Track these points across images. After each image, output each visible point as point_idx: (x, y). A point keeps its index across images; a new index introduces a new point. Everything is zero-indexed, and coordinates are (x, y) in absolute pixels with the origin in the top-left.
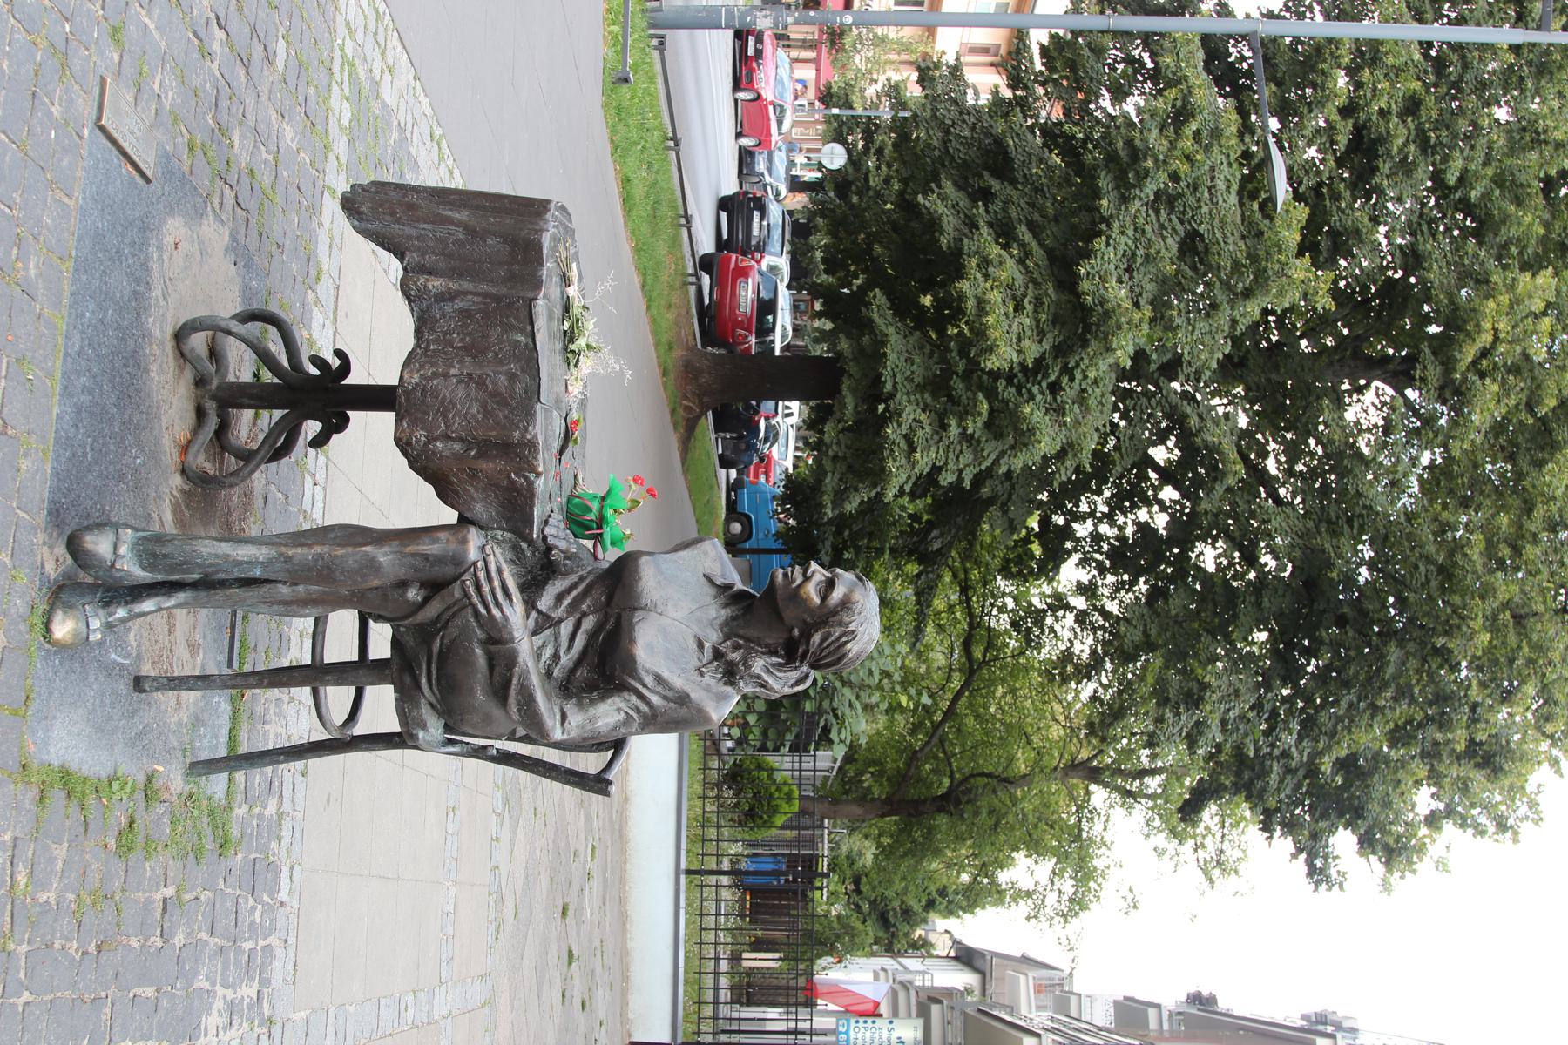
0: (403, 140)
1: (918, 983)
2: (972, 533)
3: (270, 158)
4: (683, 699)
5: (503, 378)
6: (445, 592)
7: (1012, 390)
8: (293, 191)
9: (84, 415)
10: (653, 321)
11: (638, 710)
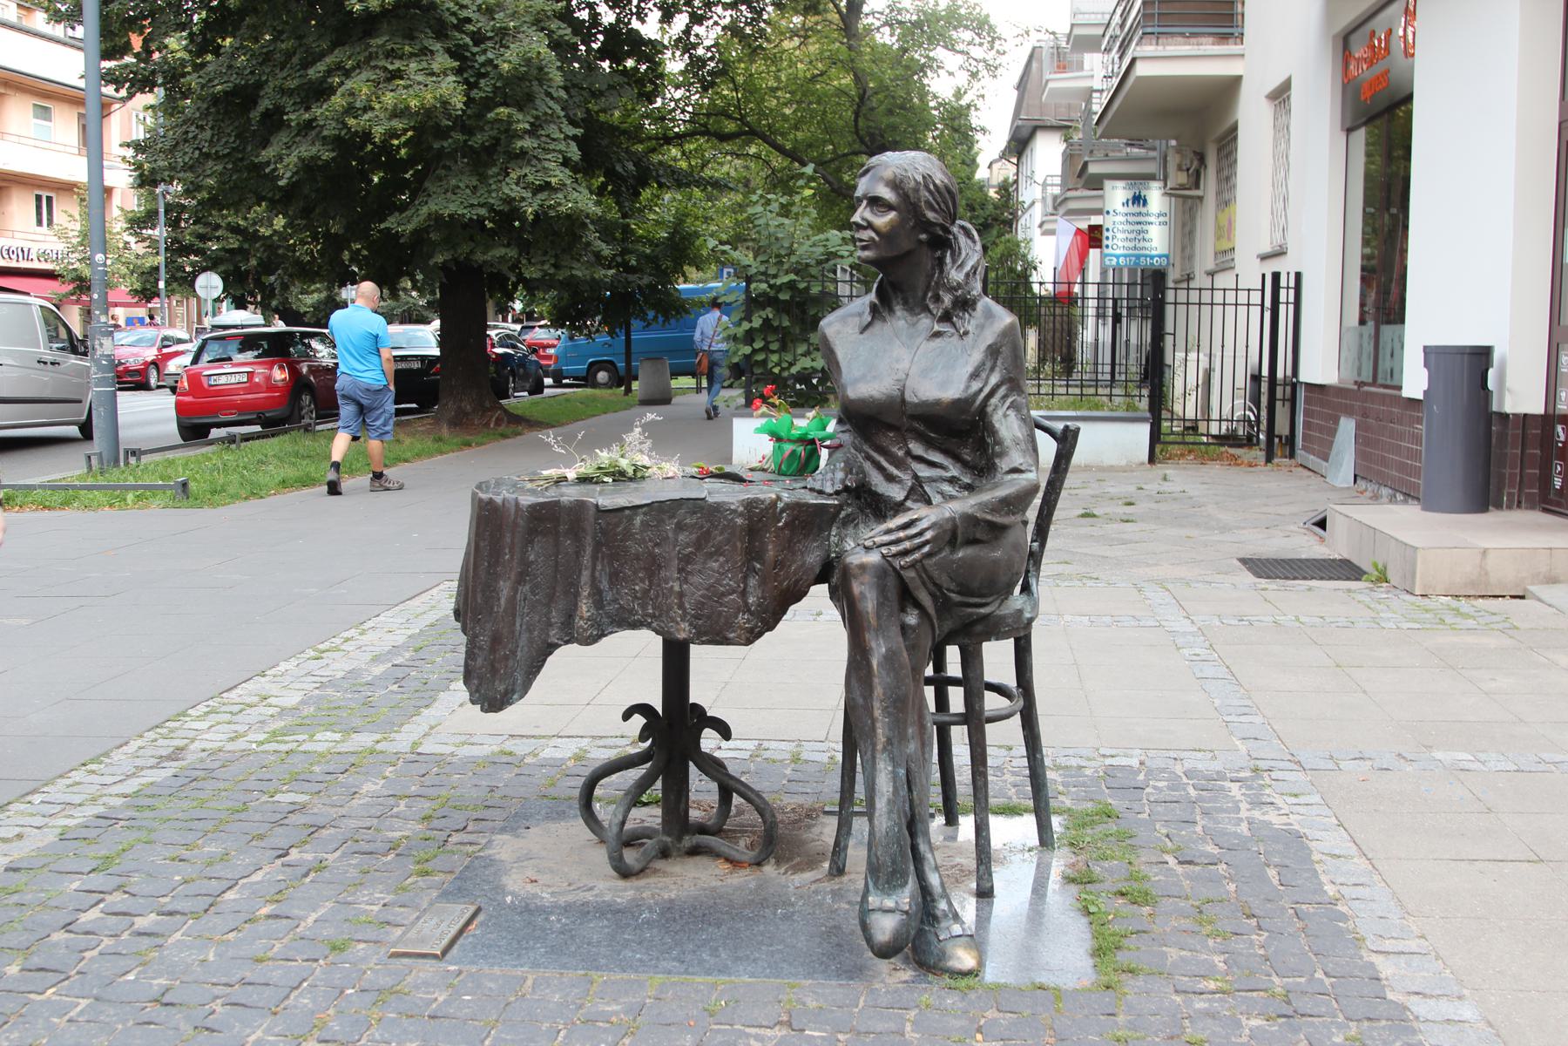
0: (332, 683)
1: (1057, 190)
2: (613, 130)
3: (403, 803)
4: (993, 351)
5: (681, 537)
6: (911, 586)
7: (482, 82)
8: (428, 780)
9: (740, 954)
10: (419, 456)
11: (1005, 397)
